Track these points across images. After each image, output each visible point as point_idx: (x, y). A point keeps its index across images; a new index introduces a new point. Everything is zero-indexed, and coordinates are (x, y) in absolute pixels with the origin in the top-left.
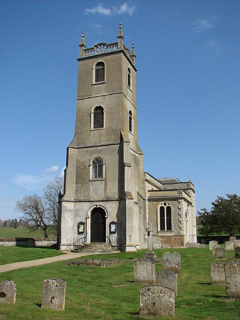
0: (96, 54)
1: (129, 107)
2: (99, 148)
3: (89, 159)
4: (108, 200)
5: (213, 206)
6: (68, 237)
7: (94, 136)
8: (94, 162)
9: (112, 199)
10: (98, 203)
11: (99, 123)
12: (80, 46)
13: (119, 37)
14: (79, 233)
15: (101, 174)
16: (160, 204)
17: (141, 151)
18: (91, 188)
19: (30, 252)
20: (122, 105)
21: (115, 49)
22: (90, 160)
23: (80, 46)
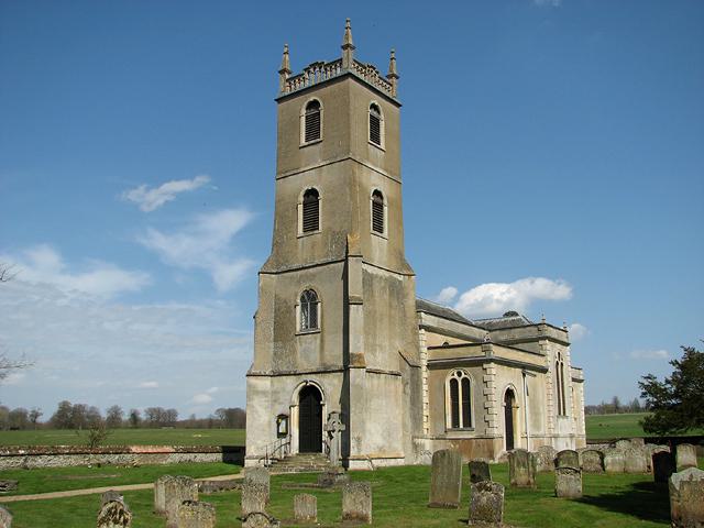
0: (308, 84)
1: (374, 180)
2: (311, 270)
3: (295, 293)
4: (325, 372)
5: (674, 369)
6: (259, 442)
7: (306, 248)
8: (303, 298)
9: (333, 369)
10: (309, 378)
11: (311, 223)
12: (343, 47)
13: (346, 47)
14: (280, 435)
15: (314, 324)
16: (451, 374)
17: (409, 269)
18: (299, 348)
19: (435, 505)
20: (352, 183)
21: (339, 72)
22: (296, 296)
23: (343, 47)
